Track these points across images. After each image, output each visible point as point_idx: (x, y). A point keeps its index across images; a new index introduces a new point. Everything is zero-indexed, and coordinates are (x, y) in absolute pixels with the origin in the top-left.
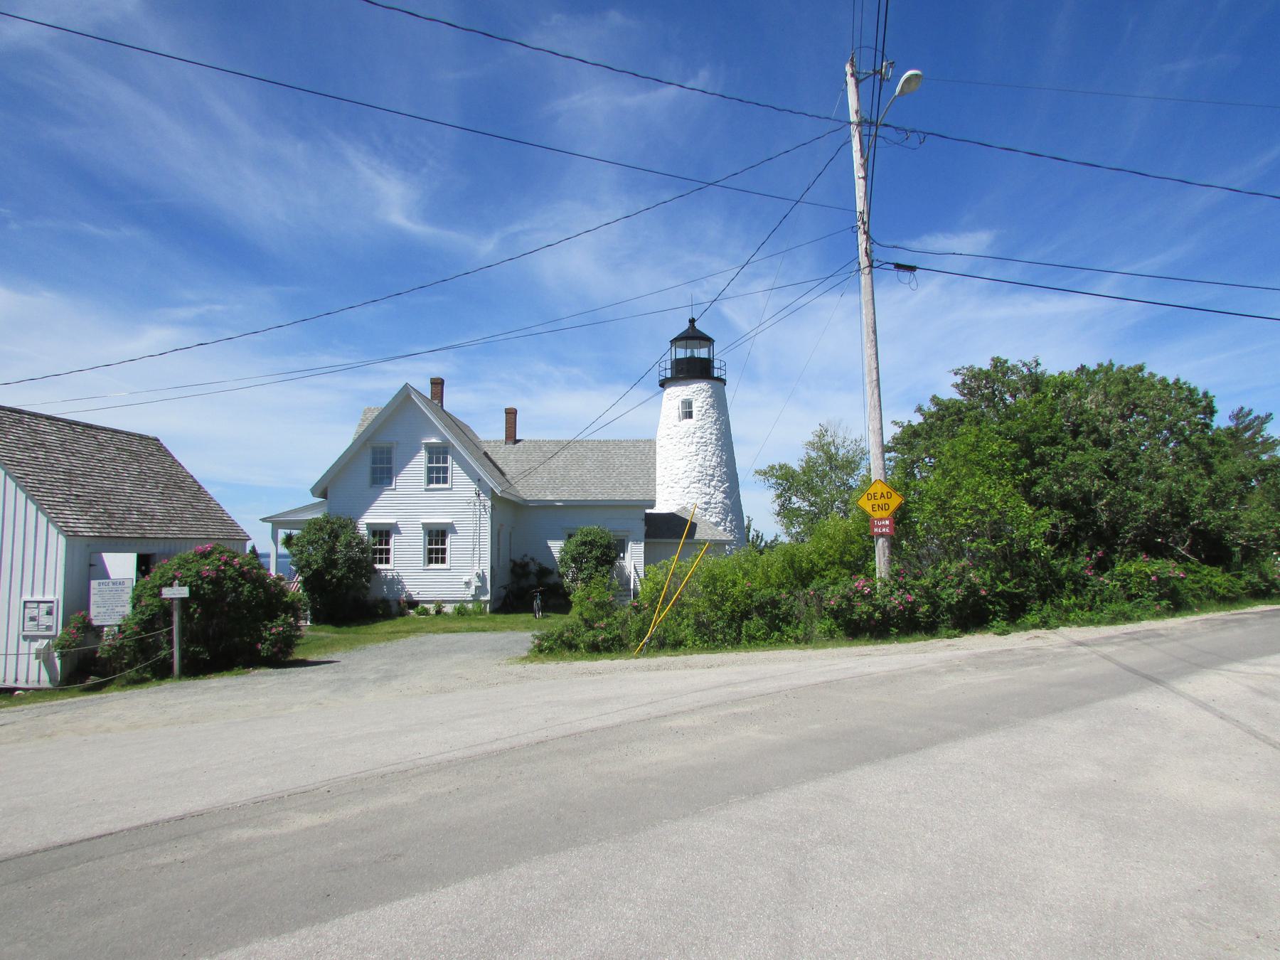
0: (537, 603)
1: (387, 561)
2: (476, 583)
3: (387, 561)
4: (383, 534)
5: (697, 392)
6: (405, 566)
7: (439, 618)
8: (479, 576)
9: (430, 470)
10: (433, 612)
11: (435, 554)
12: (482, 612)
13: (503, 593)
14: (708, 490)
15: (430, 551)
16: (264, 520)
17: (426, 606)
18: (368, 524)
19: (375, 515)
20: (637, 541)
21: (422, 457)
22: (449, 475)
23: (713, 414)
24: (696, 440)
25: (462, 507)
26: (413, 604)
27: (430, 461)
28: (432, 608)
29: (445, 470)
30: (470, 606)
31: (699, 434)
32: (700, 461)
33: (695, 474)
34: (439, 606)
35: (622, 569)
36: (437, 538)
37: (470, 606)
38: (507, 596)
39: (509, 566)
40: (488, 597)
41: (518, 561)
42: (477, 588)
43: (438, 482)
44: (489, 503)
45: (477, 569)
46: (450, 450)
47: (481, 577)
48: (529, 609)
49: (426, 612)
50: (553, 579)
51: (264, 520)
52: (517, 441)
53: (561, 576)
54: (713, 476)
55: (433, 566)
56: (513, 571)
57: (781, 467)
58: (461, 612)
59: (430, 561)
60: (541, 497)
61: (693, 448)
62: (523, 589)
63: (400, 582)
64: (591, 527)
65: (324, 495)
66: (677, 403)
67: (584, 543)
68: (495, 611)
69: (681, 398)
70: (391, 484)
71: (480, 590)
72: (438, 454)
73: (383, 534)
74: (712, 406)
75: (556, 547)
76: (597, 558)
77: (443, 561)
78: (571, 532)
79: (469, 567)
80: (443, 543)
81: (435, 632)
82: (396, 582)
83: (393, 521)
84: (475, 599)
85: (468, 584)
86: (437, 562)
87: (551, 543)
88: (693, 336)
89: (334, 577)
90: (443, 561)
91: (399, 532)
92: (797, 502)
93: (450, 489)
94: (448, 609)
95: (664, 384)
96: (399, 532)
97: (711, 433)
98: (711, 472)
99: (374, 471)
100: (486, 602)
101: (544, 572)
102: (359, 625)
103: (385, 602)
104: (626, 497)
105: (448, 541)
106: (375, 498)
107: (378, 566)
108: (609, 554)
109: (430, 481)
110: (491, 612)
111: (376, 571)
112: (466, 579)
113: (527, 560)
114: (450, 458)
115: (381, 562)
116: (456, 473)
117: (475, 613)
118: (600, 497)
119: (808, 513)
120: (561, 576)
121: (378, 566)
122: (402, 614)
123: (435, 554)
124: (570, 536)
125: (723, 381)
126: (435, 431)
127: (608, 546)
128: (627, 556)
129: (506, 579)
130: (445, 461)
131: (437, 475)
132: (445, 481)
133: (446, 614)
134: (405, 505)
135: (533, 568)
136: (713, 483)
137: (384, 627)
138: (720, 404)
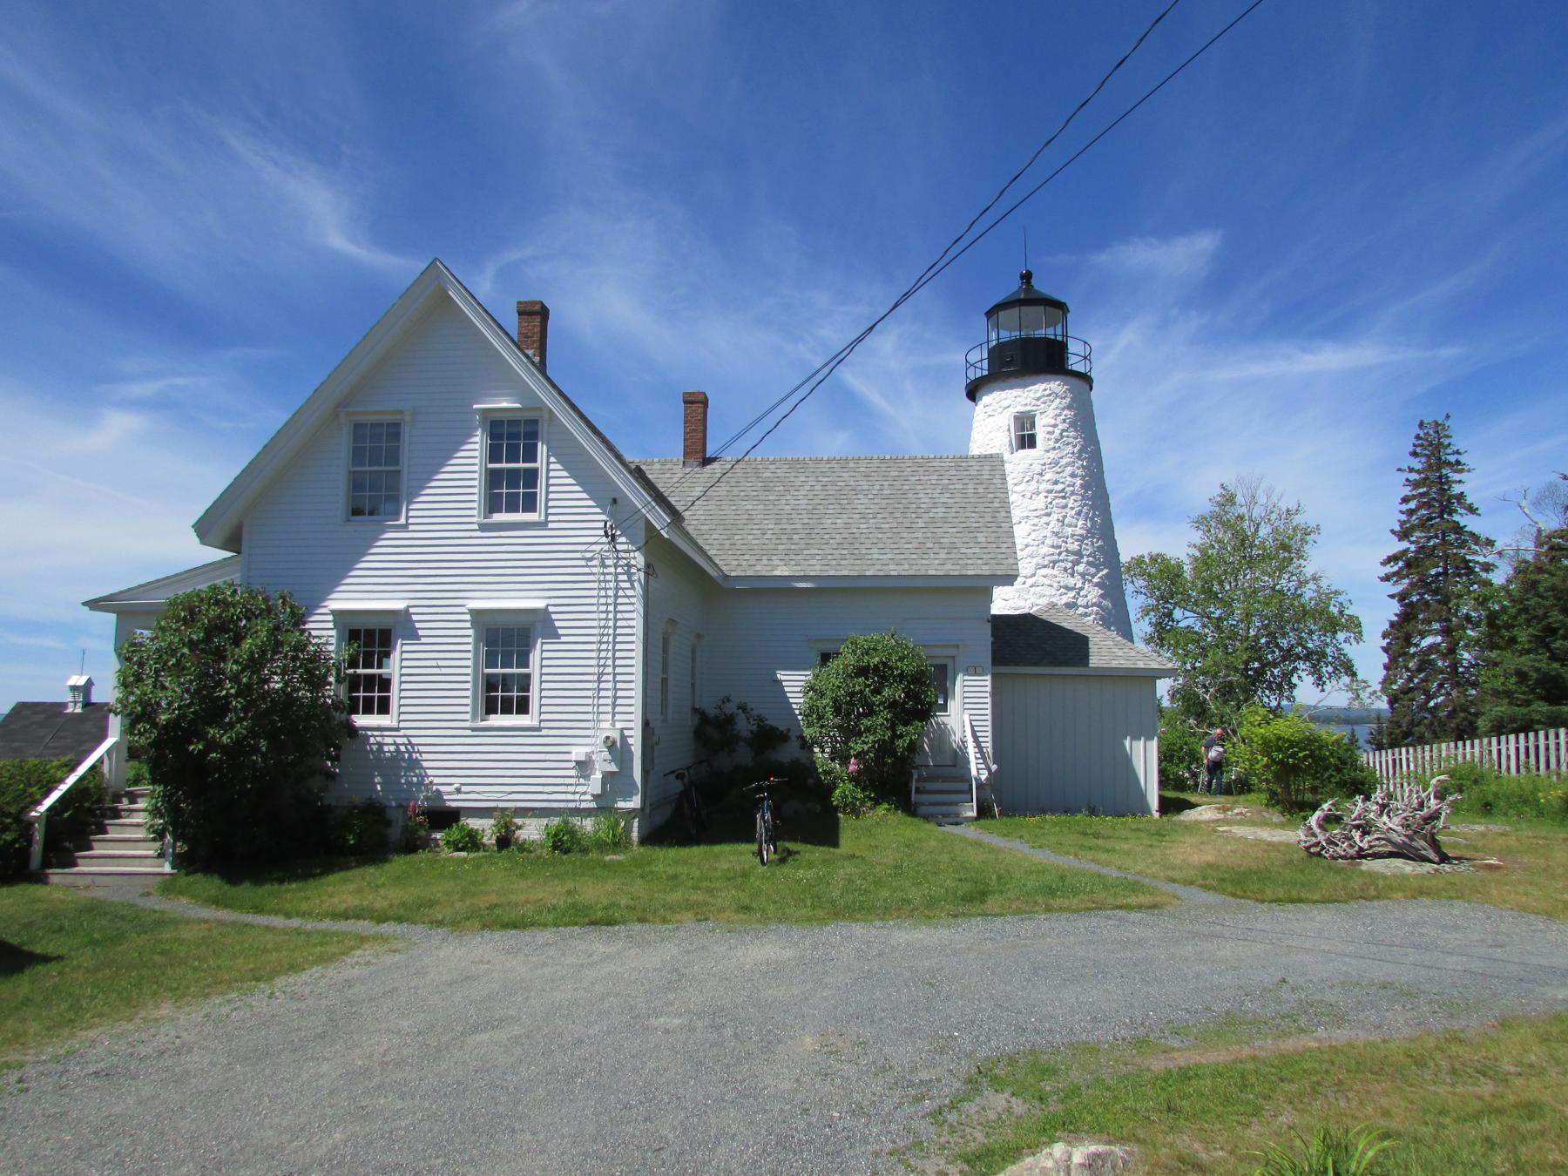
0: (763, 820)
1: (384, 708)
2: (603, 764)
3: (384, 708)
4: (372, 638)
5: (1042, 398)
6: (428, 725)
7: (503, 859)
8: (610, 745)
9: (493, 479)
10: (489, 839)
11: (503, 695)
12: (619, 843)
13: (677, 786)
14: (1071, 581)
15: (491, 684)
16: (94, 604)
17: (474, 823)
18: (338, 614)
19: (360, 594)
20: (975, 671)
21: (477, 445)
22: (541, 490)
23: (1074, 440)
24: (1043, 487)
25: (568, 568)
26: (444, 817)
27: (494, 455)
28: (485, 827)
29: (531, 477)
30: (588, 824)
31: (1049, 476)
32: (1054, 525)
33: (1045, 550)
34: (507, 821)
35: (943, 733)
36: (507, 642)
37: (588, 824)
38: (684, 795)
39: (691, 721)
40: (635, 802)
41: (712, 712)
42: (607, 777)
43: (512, 508)
44: (639, 560)
45: (607, 729)
46: (543, 429)
47: (618, 749)
48: (744, 833)
49: (471, 842)
50: (788, 753)
51: (94, 604)
52: (707, 461)
53: (806, 746)
54: (1079, 553)
55: (498, 720)
56: (699, 734)
57: (1154, 559)
58: (564, 843)
59: (491, 709)
60: (761, 569)
61: (1040, 502)
62: (735, 780)
63: (415, 764)
64: (872, 634)
65: (233, 542)
66: (1006, 420)
67: (862, 671)
68: (656, 836)
69: (1012, 411)
70: (397, 514)
71: (615, 782)
72: (513, 438)
73: (372, 638)
74: (1073, 424)
75: (795, 684)
76: (893, 705)
77: (523, 707)
78: (828, 647)
79: (584, 731)
80: (524, 662)
81: (456, 924)
82: (405, 763)
83: (399, 605)
84: (603, 806)
85: (584, 766)
86: (507, 710)
87: (781, 675)
88: (1029, 298)
89: (212, 745)
90: (523, 707)
91: (413, 635)
92: (1185, 618)
93: (543, 525)
94: (531, 831)
95: (973, 393)
96: (413, 635)
97: (1071, 476)
98: (1075, 547)
99: (356, 484)
100: (631, 813)
101: (769, 737)
102: (281, 881)
103: (374, 813)
104: (950, 569)
105: (535, 657)
106: (360, 550)
107: (361, 720)
108: (921, 695)
109: (493, 505)
110: (644, 841)
111: (353, 731)
112: (578, 753)
113: (730, 708)
114: (542, 449)
115: (368, 710)
116: (558, 485)
117: (601, 846)
118: (893, 570)
119: (1411, 584)
120: (806, 746)
121: (361, 720)
122: (412, 844)
123: (503, 695)
124: (825, 658)
125: (1086, 378)
126: (513, 384)
127: (918, 678)
128: (954, 705)
129: (680, 754)
130: (531, 456)
131: (510, 490)
132: (530, 505)
133: (523, 847)
134: (433, 566)
135: (744, 726)
136: (1080, 568)
137: (344, 889)
138: (1083, 421)
